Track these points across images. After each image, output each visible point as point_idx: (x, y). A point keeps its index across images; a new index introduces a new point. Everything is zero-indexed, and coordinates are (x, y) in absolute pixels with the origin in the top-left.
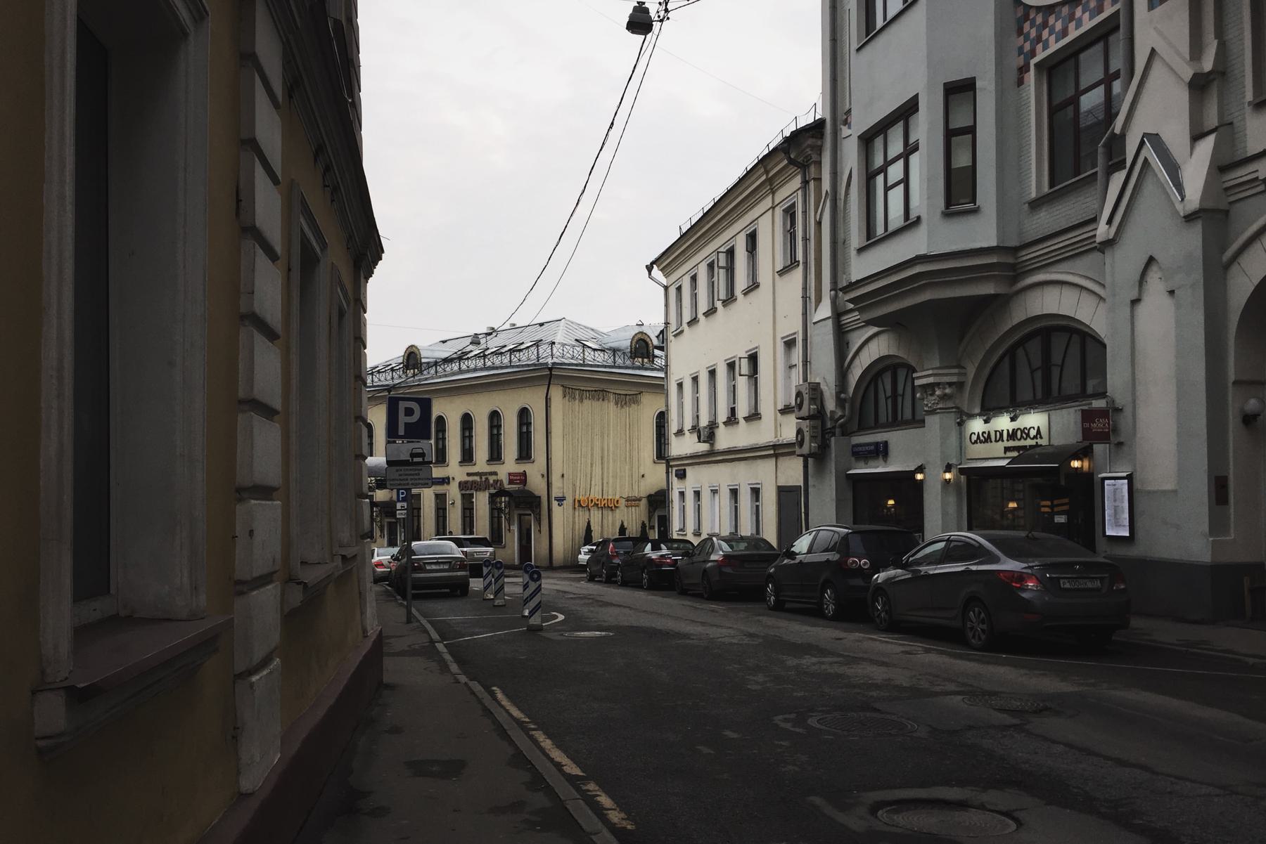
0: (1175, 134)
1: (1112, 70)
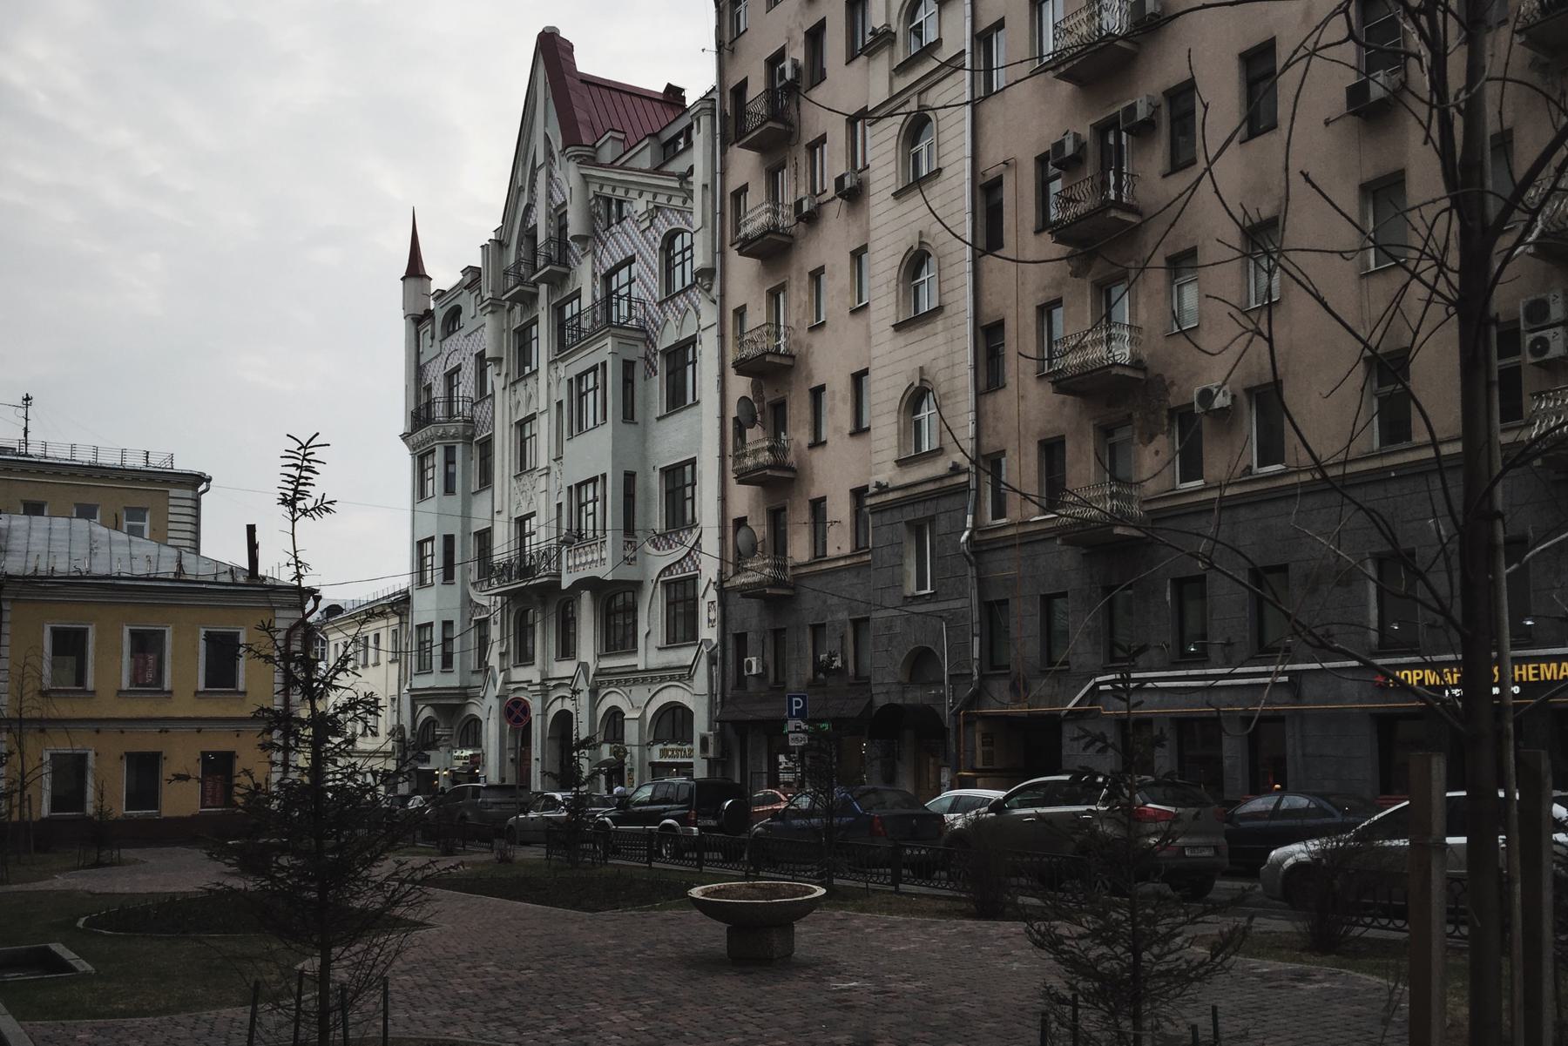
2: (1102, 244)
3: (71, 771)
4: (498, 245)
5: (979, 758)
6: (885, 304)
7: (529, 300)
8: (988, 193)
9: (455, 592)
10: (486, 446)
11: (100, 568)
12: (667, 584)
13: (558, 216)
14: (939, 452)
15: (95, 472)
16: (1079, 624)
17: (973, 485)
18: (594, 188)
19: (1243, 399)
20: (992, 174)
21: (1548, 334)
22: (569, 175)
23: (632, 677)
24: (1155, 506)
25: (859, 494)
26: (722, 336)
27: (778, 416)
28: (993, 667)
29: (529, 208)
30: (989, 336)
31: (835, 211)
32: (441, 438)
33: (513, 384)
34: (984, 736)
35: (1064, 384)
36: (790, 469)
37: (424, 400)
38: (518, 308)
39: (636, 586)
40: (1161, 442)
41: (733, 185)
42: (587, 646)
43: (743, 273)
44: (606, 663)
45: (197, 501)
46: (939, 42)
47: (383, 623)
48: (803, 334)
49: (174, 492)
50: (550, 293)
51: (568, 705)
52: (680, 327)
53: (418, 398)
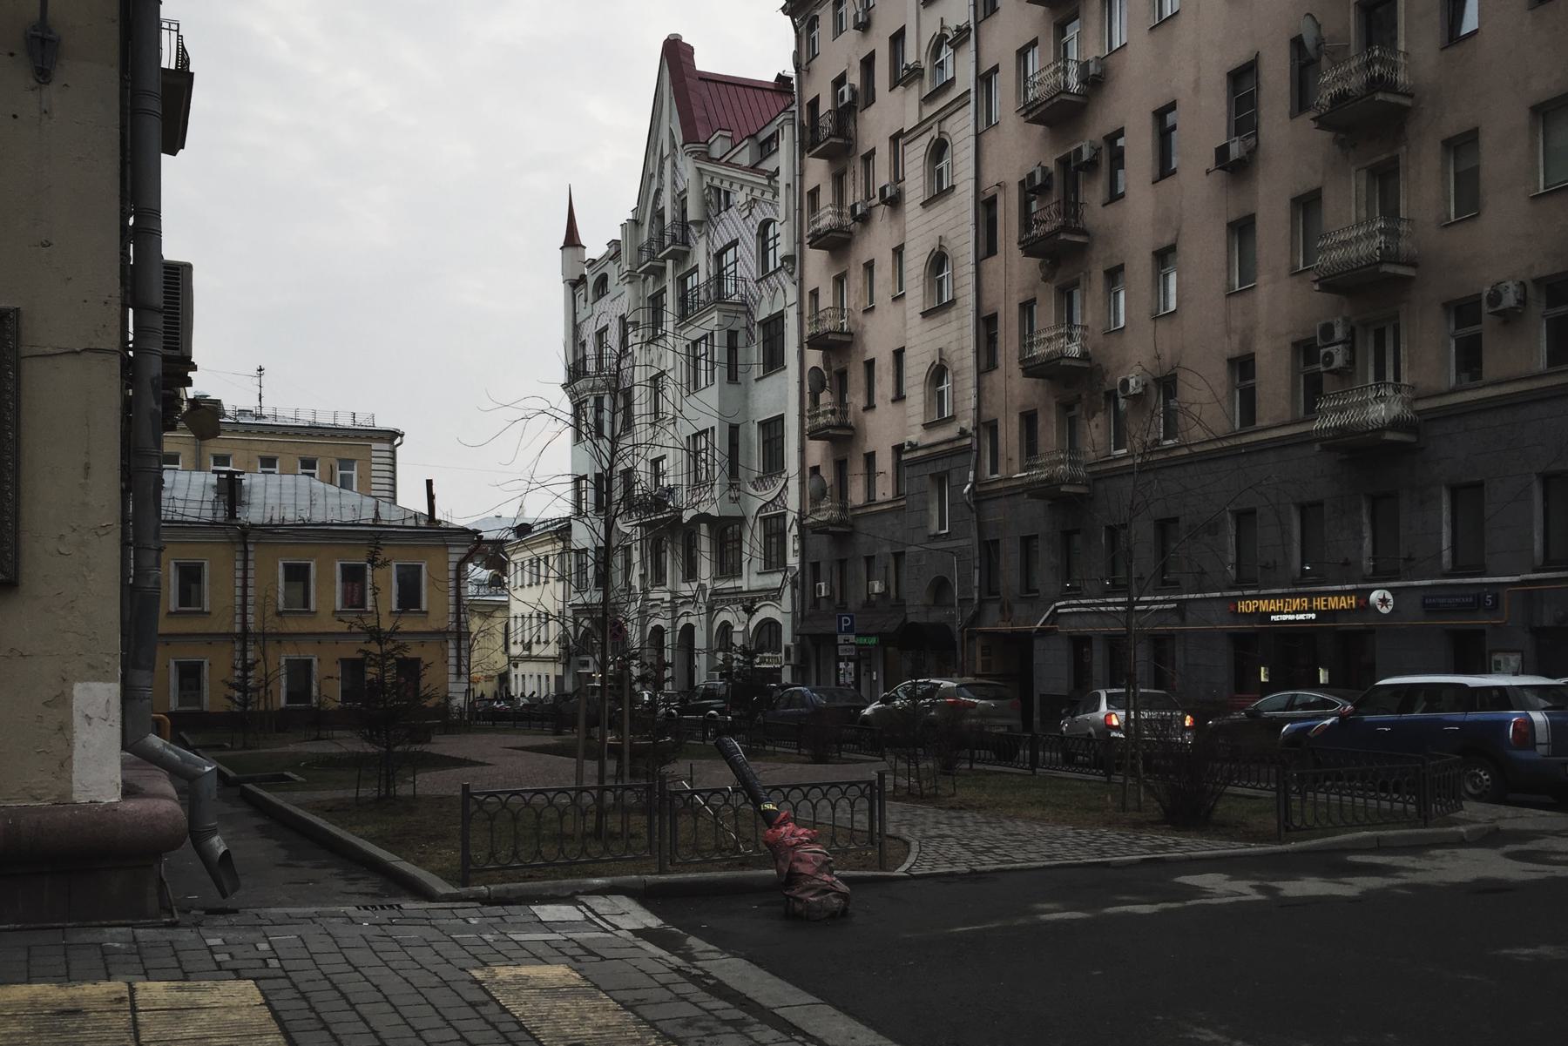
2: (1063, 252)
3: (300, 671)
4: (636, 223)
5: (979, 664)
6: (916, 296)
7: (659, 273)
8: (986, 207)
10: (628, 394)
11: (318, 517)
12: (764, 519)
13: (681, 200)
14: (953, 418)
15: (315, 431)
16: (1046, 558)
17: (975, 447)
18: (707, 179)
19: (1153, 389)
20: (989, 193)
21: (1333, 349)
22: (688, 167)
23: (736, 597)
24: (1097, 468)
25: (898, 449)
26: (801, 313)
27: (841, 380)
28: (990, 593)
29: (658, 192)
30: (987, 325)
31: (881, 212)
32: (592, 390)
33: (649, 342)
34: (983, 648)
35: (1032, 369)
36: (850, 428)
37: (580, 355)
38: (651, 279)
39: (742, 520)
40: (1100, 418)
41: (809, 186)
42: (705, 569)
43: (816, 260)
44: (719, 585)
45: (394, 452)
46: (953, 79)
47: (549, 547)
48: (859, 316)
49: (375, 446)
50: (675, 267)
51: (692, 620)
52: (772, 303)
53: (575, 353)
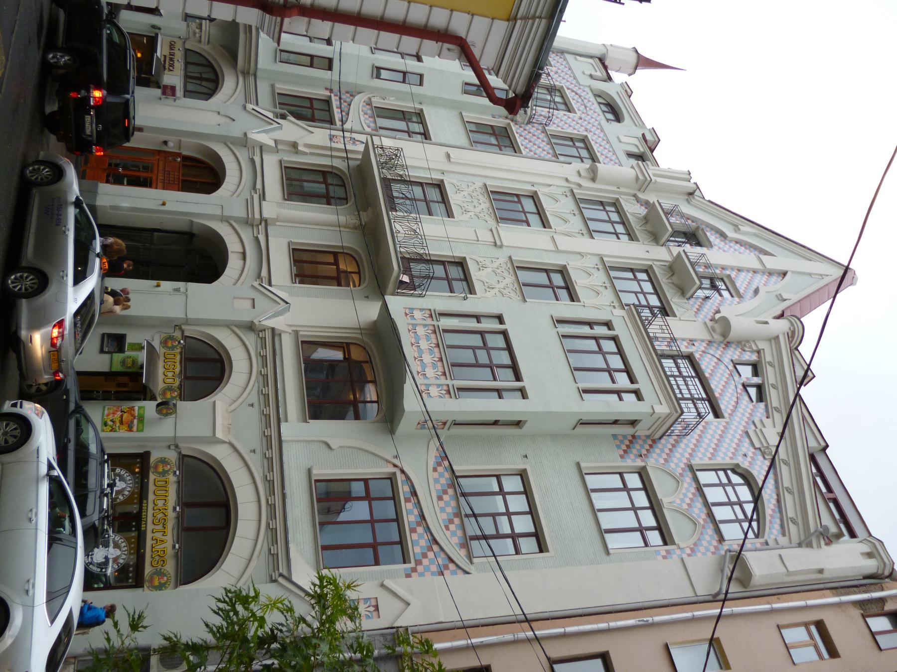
0: (279, 135)
1: (624, 395)
9: (364, 78)
12: (392, 479)
